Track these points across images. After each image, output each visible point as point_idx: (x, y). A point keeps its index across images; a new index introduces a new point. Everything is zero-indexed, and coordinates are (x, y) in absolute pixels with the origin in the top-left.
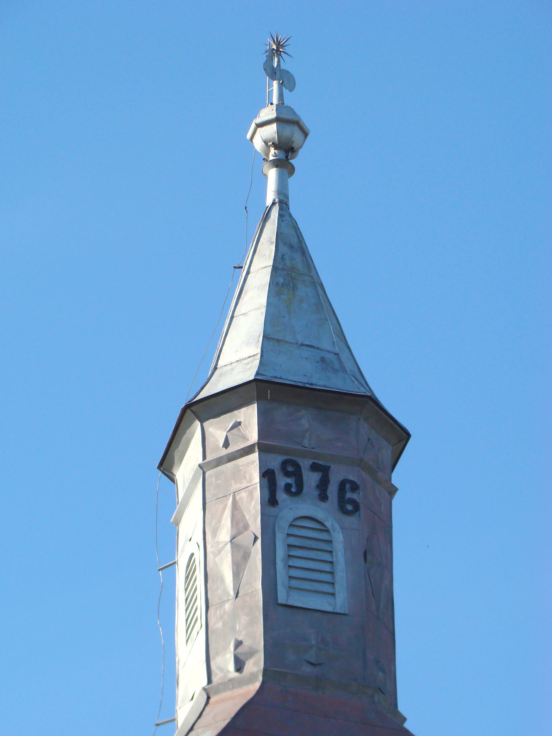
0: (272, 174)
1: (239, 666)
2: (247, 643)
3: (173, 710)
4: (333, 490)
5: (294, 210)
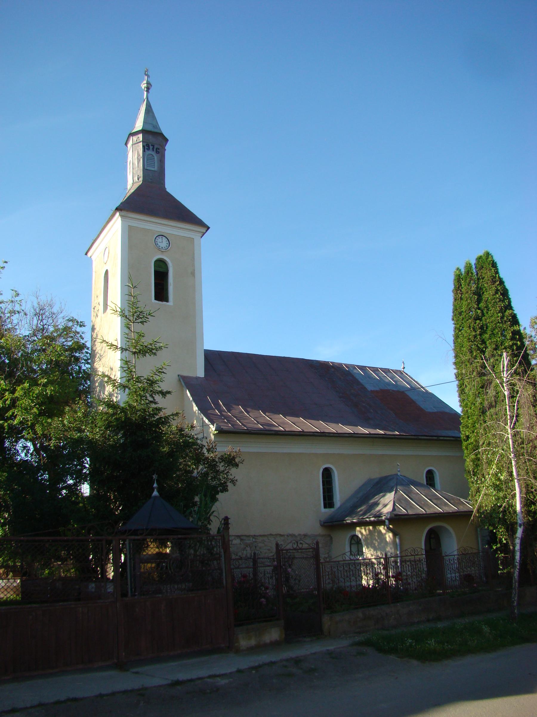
0: (145, 93)
1: (138, 179)
4: (155, 149)
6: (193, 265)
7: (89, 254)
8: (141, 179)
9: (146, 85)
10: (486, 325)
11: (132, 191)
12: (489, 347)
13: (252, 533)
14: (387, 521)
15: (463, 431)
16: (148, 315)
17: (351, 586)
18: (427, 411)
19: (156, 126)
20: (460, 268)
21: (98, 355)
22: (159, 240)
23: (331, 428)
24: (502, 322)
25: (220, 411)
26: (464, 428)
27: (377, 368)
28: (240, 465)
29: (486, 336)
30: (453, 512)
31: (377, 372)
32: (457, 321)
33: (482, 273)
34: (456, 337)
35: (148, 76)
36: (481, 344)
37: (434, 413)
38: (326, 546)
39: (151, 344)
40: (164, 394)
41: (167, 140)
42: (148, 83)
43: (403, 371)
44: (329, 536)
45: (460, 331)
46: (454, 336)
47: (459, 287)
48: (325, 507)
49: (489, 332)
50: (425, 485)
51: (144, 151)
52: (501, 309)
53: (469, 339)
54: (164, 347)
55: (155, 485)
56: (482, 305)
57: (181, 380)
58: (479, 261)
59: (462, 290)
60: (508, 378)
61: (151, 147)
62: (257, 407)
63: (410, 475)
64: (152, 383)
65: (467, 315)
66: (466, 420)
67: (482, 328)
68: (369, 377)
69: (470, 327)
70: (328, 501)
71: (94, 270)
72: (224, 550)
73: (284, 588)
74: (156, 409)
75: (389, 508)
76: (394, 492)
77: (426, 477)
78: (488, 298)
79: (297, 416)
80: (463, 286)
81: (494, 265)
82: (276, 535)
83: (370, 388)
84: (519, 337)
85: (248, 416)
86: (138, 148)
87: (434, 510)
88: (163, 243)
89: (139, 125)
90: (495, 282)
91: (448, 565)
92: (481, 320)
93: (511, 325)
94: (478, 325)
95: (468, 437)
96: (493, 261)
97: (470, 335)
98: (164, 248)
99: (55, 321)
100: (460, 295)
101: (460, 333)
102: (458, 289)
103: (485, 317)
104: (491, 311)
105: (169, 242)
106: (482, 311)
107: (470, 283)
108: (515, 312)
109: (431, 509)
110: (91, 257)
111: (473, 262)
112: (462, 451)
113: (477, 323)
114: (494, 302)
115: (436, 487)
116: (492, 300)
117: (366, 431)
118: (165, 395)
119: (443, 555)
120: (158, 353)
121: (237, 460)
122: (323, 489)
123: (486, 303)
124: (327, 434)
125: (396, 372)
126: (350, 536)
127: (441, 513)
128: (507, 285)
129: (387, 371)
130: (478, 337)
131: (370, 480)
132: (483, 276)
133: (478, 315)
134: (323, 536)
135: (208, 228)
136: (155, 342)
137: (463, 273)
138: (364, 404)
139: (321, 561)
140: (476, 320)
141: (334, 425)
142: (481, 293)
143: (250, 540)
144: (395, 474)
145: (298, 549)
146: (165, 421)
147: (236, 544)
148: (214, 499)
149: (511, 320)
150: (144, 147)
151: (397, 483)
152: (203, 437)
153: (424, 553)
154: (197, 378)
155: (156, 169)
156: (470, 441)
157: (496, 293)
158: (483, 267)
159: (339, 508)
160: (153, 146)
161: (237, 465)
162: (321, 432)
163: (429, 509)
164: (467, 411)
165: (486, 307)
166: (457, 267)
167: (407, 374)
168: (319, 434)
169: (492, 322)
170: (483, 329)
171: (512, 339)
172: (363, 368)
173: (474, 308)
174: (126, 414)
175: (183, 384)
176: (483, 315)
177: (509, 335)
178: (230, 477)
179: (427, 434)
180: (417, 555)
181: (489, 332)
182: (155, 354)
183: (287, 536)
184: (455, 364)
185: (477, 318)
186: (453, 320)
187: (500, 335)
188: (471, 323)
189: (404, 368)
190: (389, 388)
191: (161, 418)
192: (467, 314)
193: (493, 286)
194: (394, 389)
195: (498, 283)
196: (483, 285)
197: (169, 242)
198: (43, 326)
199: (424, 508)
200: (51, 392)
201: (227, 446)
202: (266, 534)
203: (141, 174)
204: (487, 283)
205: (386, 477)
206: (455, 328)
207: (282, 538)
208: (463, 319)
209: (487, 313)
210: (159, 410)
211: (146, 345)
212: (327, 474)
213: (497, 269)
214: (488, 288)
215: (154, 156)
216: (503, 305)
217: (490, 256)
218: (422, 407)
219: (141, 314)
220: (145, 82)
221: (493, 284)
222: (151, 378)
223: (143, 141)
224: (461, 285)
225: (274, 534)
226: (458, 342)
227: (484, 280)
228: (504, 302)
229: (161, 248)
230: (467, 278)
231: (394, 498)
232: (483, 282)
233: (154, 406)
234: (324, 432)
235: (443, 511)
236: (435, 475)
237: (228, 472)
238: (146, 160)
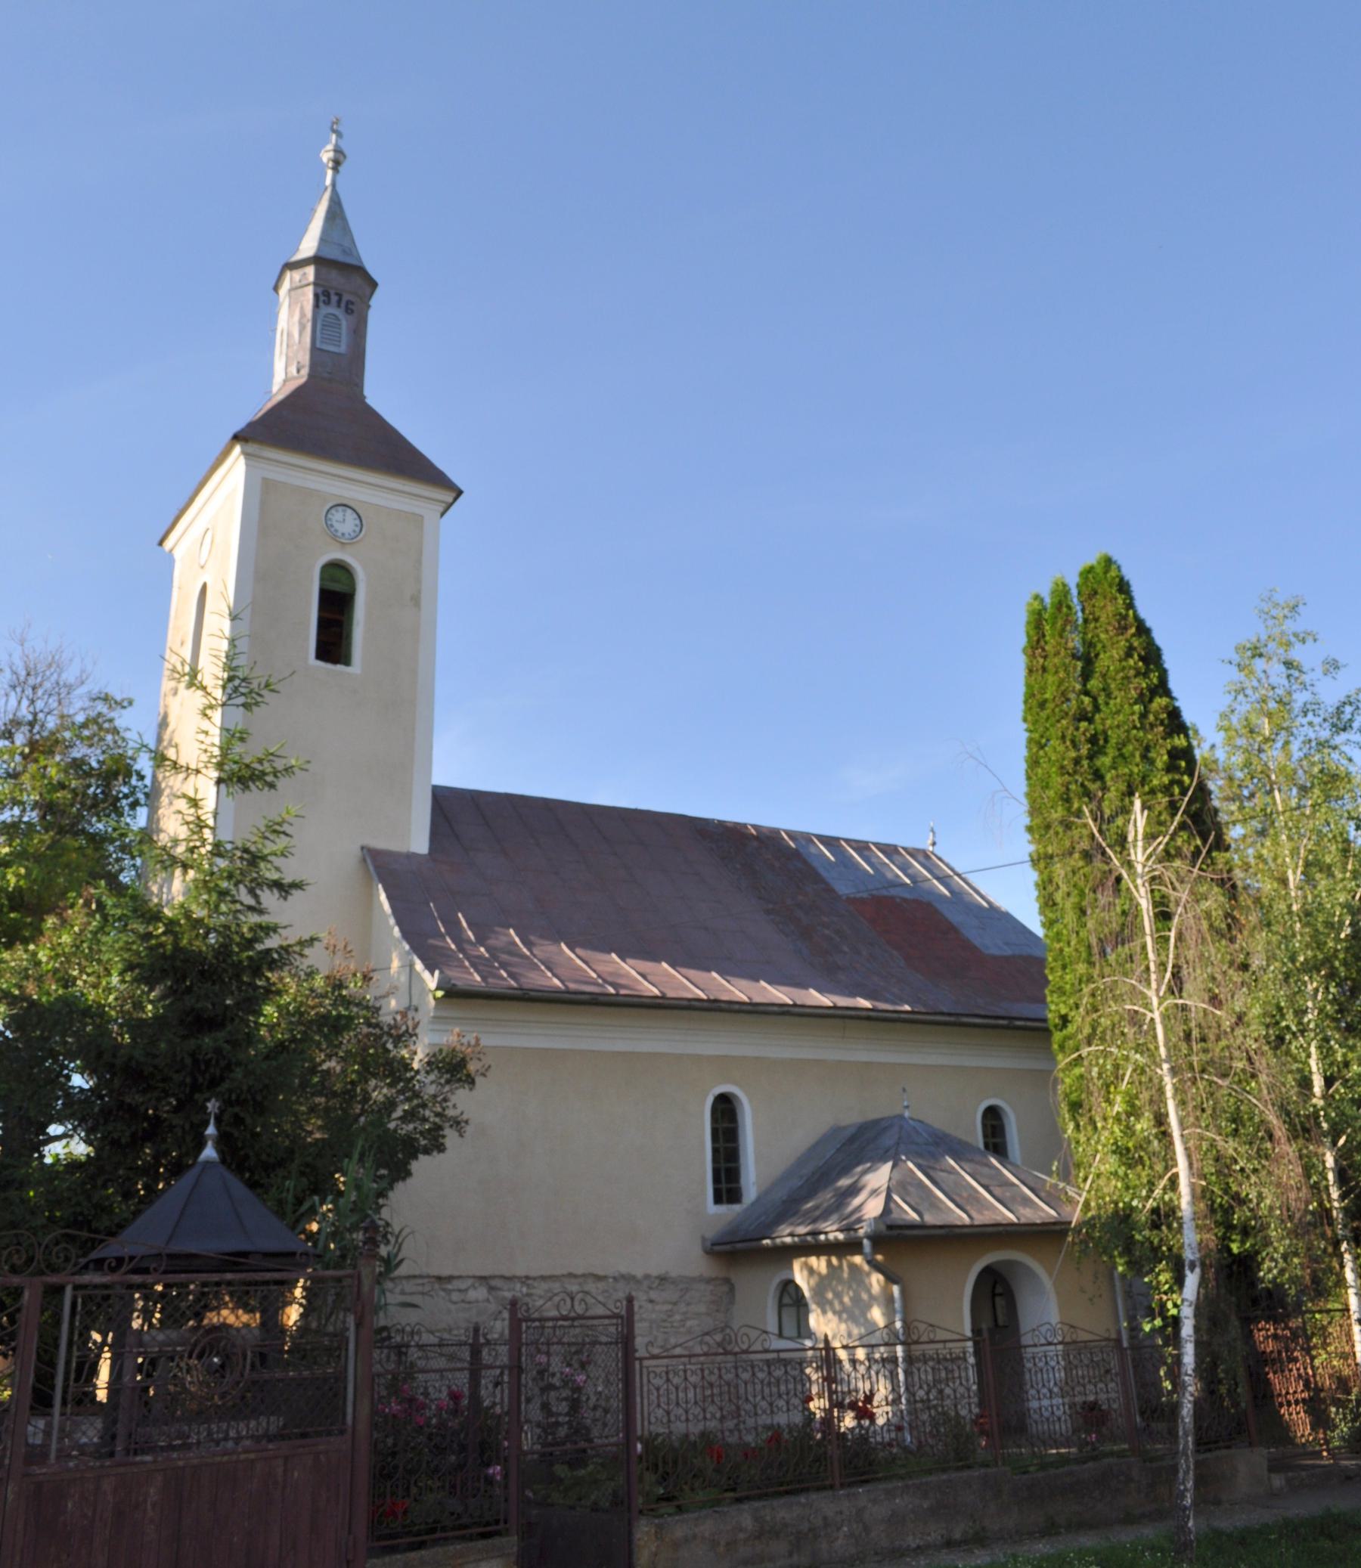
0: (330, 173)
1: (298, 371)
2: (302, 363)
3: (271, 388)
4: (343, 305)
5: (339, 188)
6: (418, 580)
7: (168, 544)
8: (305, 372)
9: (331, 155)
10: (1105, 732)
11: (280, 397)
12: (1112, 789)
13: (520, 1272)
14: (866, 1242)
15: (1052, 1002)
16: (262, 686)
17: (1063, 1397)
18: (987, 952)
19: (351, 249)
20: (1042, 595)
21: (167, 792)
22: (337, 515)
23: (737, 990)
24: (1142, 727)
25: (459, 940)
26: (1055, 995)
27: (867, 842)
28: (479, 1080)
29: (1104, 761)
30: (1043, 1224)
31: (866, 853)
32: (1035, 722)
33: (1094, 606)
34: (1033, 763)
35: (339, 135)
36: (1094, 781)
37: (1007, 959)
38: (717, 1311)
39: (260, 761)
40: (284, 888)
41: (374, 285)
42: (338, 150)
43: (932, 853)
44: (727, 1281)
45: (1042, 747)
46: (1026, 761)
47: (1038, 641)
48: (718, 1199)
49: (1111, 752)
50: (979, 1149)
51: (316, 306)
52: (1141, 695)
53: (1062, 767)
54: (302, 769)
55: (211, 1130)
56: (1094, 684)
57: (369, 861)
58: (1086, 579)
59: (1047, 648)
60: (1150, 863)
61: (334, 298)
62: (557, 935)
63: (938, 1118)
64: (254, 859)
65: (1057, 710)
66: (1059, 974)
67: (1093, 740)
68: (844, 861)
69: (1063, 737)
70: (727, 1187)
71: (176, 583)
72: (355, 1319)
73: (526, 1433)
74: (260, 926)
75: (873, 1208)
76: (890, 1164)
77: (984, 1126)
78: (1108, 667)
79: (656, 959)
80: (1047, 638)
81: (1124, 587)
82: (584, 1275)
83: (843, 889)
84: (1188, 763)
85: (528, 953)
86: (302, 298)
87: (994, 1217)
88: (346, 523)
89: (309, 246)
90: (1126, 628)
91: (677, 1388)
92: (1090, 721)
93: (1166, 733)
94: (1084, 734)
95: (1065, 1020)
96: (1122, 579)
97: (1064, 759)
98: (347, 536)
99: (65, 702)
100: (1041, 661)
101: (1041, 753)
102: (1036, 644)
103: (1102, 715)
104: (1116, 698)
105: (361, 521)
106: (1095, 699)
107: (1063, 630)
108: (1177, 704)
109: (986, 1213)
110: (171, 551)
111: (1073, 581)
112: (1053, 1059)
113: (1082, 729)
114: (1123, 678)
115: (1010, 1154)
116: (1117, 672)
117: (825, 1000)
118: (287, 892)
119: (1026, 1340)
120: (282, 783)
121: (472, 1067)
122: (715, 1151)
123: (1105, 680)
124: (723, 1005)
125: (914, 853)
126: (781, 1282)
127: (1013, 1224)
128: (1160, 638)
129: (890, 850)
130: (1085, 763)
131: (836, 1130)
132: (1097, 614)
133: (1085, 709)
134: (709, 1281)
135: (460, 493)
136: (272, 754)
137: (1049, 606)
138: (827, 932)
139: (637, 1355)
140: (1080, 720)
141: (744, 983)
142: (1093, 655)
143: (514, 1290)
144: (895, 1117)
145: (573, 1319)
146: (279, 959)
147: (477, 1301)
148: (401, 1172)
149: (1166, 722)
150: (316, 296)
151: (899, 1138)
152: (407, 1005)
153: (969, 1334)
154: (411, 856)
155: (343, 348)
156: (1071, 1029)
157: (1129, 654)
158: (1096, 593)
159: (753, 1204)
160: (339, 295)
161: (470, 1081)
162: (709, 1001)
163: (980, 1212)
164: (1061, 950)
165: (1104, 690)
166: (1034, 591)
167: (940, 859)
168: (706, 1005)
169: (1118, 726)
170: (1098, 744)
171: (1170, 768)
172: (830, 842)
173: (1073, 691)
174: (177, 938)
175: (371, 868)
176: (1097, 708)
177: (1162, 759)
178: (450, 1113)
179: (983, 1013)
180: (917, 1342)
181: (1111, 752)
182: (272, 786)
183: (615, 1278)
184: (1030, 829)
185: (1083, 716)
186: (1025, 720)
187: (1138, 759)
188: (1067, 728)
189: (934, 844)
190: (893, 892)
191: (268, 951)
192: (1057, 706)
193: (1120, 637)
194: (907, 896)
195: (1133, 630)
196: (1098, 636)
197: (361, 521)
198: (35, 714)
199: (968, 1208)
200: (18, 881)
201: (447, 1031)
202: (558, 1272)
203: (305, 359)
204: (1107, 631)
205: (876, 1122)
206: (1030, 741)
207: (601, 1285)
208: (1048, 718)
209: (1107, 704)
210: (269, 930)
211: (247, 761)
212: (725, 1109)
213: (1131, 599)
214: (1108, 644)
215: (339, 320)
216: (1144, 685)
217: (1113, 567)
218: (977, 942)
219: (244, 684)
220: (330, 147)
221: (1122, 634)
222: (253, 849)
223: (316, 284)
224: (1044, 636)
225: (580, 1272)
226: (1036, 775)
227: (1098, 625)
228: (1149, 678)
229: (339, 534)
230: (1056, 618)
231: (890, 1179)
232: (1096, 628)
233: (254, 919)
234: (716, 1001)
235: (1018, 1219)
236: (1006, 1122)
237: (445, 1100)
238: (321, 326)
